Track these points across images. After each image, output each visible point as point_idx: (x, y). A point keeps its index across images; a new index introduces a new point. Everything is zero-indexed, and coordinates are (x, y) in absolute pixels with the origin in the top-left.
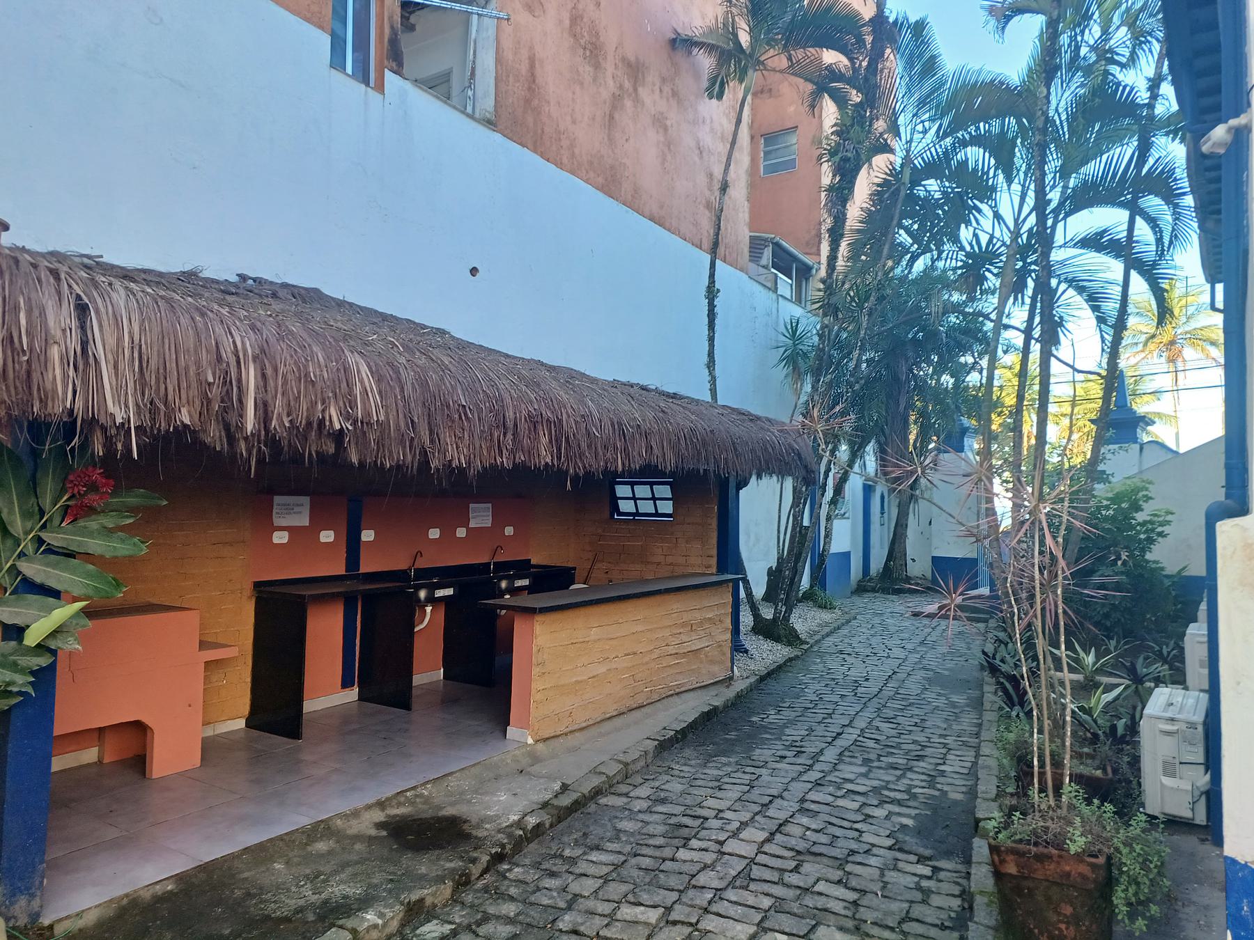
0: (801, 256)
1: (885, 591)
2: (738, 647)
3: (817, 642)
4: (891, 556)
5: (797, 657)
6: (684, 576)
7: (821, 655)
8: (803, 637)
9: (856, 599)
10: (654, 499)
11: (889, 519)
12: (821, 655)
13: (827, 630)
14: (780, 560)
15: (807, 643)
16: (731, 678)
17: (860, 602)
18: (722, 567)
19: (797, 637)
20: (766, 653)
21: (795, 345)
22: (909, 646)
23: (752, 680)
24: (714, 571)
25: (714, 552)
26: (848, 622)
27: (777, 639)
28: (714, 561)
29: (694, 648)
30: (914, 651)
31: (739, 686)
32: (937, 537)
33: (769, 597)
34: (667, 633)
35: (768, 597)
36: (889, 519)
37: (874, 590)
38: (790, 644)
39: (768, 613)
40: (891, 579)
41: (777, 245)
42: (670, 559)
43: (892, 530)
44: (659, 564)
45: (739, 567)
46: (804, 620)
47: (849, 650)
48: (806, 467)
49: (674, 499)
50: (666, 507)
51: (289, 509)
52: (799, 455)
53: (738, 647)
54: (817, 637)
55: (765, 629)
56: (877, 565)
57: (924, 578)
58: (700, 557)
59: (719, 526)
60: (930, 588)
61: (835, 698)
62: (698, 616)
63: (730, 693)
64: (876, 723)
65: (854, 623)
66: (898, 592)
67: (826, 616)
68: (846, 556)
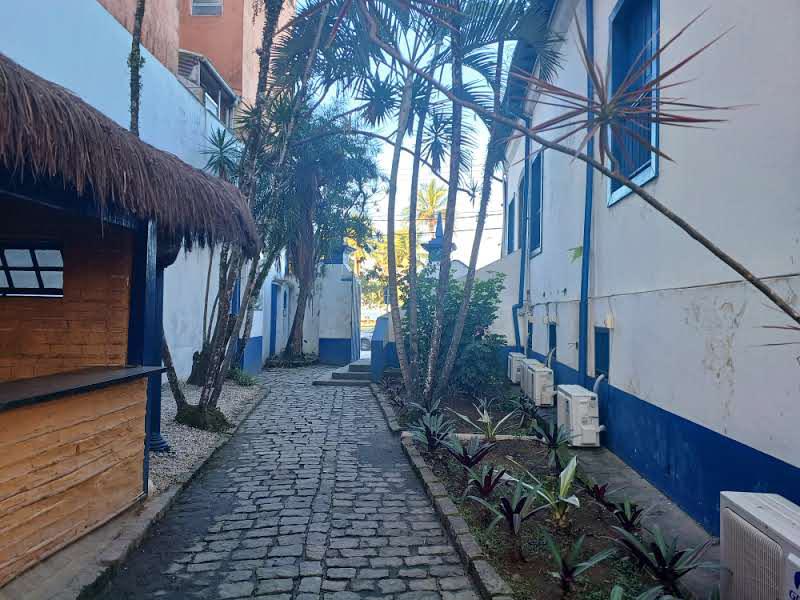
0: (229, 89)
1: (287, 366)
2: (154, 443)
3: (243, 422)
4: (291, 340)
5: (224, 444)
6: (79, 372)
7: (248, 437)
8: (229, 418)
9: (265, 373)
10: (37, 269)
11: (289, 311)
12: (248, 437)
13: (250, 407)
14: (206, 345)
15: (234, 426)
16: (143, 499)
17: (272, 375)
18: (134, 358)
19: (224, 421)
20: (189, 446)
21: (221, 153)
22: (325, 417)
23: (172, 493)
24: (123, 362)
25: (124, 338)
26: (266, 396)
27: (203, 427)
28: (123, 351)
29: (82, 478)
30: (330, 422)
31: (155, 507)
32: (321, 324)
33: (196, 378)
34: (22, 472)
35: (192, 380)
36: (289, 311)
37: (279, 365)
38: (216, 430)
39: (193, 398)
40: (291, 357)
41: (204, 65)
42: (57, 350)
43: (292, 319)
44: (40, 356)
45: (160, 353)
46: (230, 401)
47: (274, 429)
48: (247, 233)
49: (67, 270)
50: (55, 280)
51: (366, 357)
52: (240, 217)
53: (154, 443)
54: (242, 417)
55: (190, 417)
56: (281, 344)
57: (313, 354)
58: (103, 345)
59: (131, 303)
60: (316, 362)
61: (275, 504)
62: (90, 431)
63: (138, 526)
64: (336, 544)
65: (271, 397)
66: (296, 366)
67: (246, 393)
68: (259, 339)
